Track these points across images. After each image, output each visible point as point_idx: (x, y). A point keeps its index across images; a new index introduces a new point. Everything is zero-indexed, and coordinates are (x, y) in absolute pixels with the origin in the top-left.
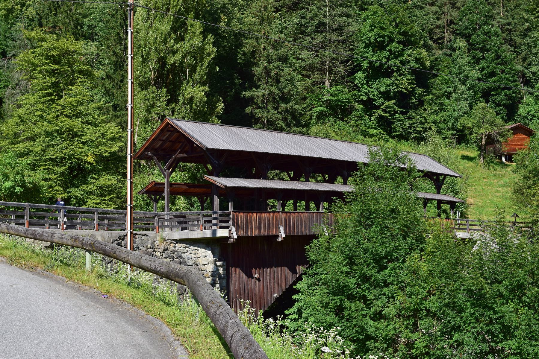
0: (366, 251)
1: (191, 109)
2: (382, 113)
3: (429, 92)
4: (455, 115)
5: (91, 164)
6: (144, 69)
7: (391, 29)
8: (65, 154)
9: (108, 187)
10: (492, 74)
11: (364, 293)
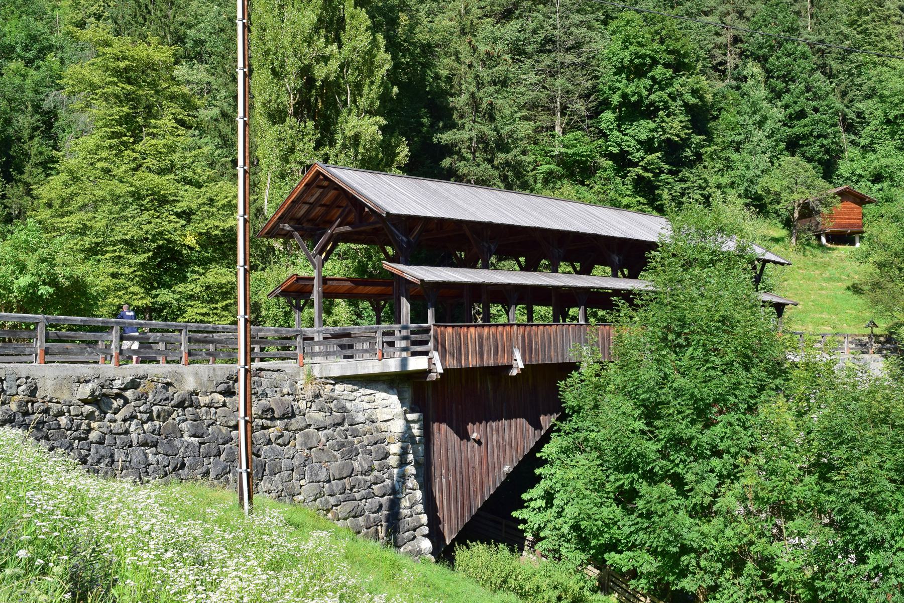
0: (679, 393)
1: (356, 156)
2: (641, 172)
3: (710, 140)
4: (749, 174)
5: (192, 249)
6: (276, 89)
7: (655, 45)
8: (147, 233)
9: (220, 286)
10: (802, 115)
11: (676, 469)
